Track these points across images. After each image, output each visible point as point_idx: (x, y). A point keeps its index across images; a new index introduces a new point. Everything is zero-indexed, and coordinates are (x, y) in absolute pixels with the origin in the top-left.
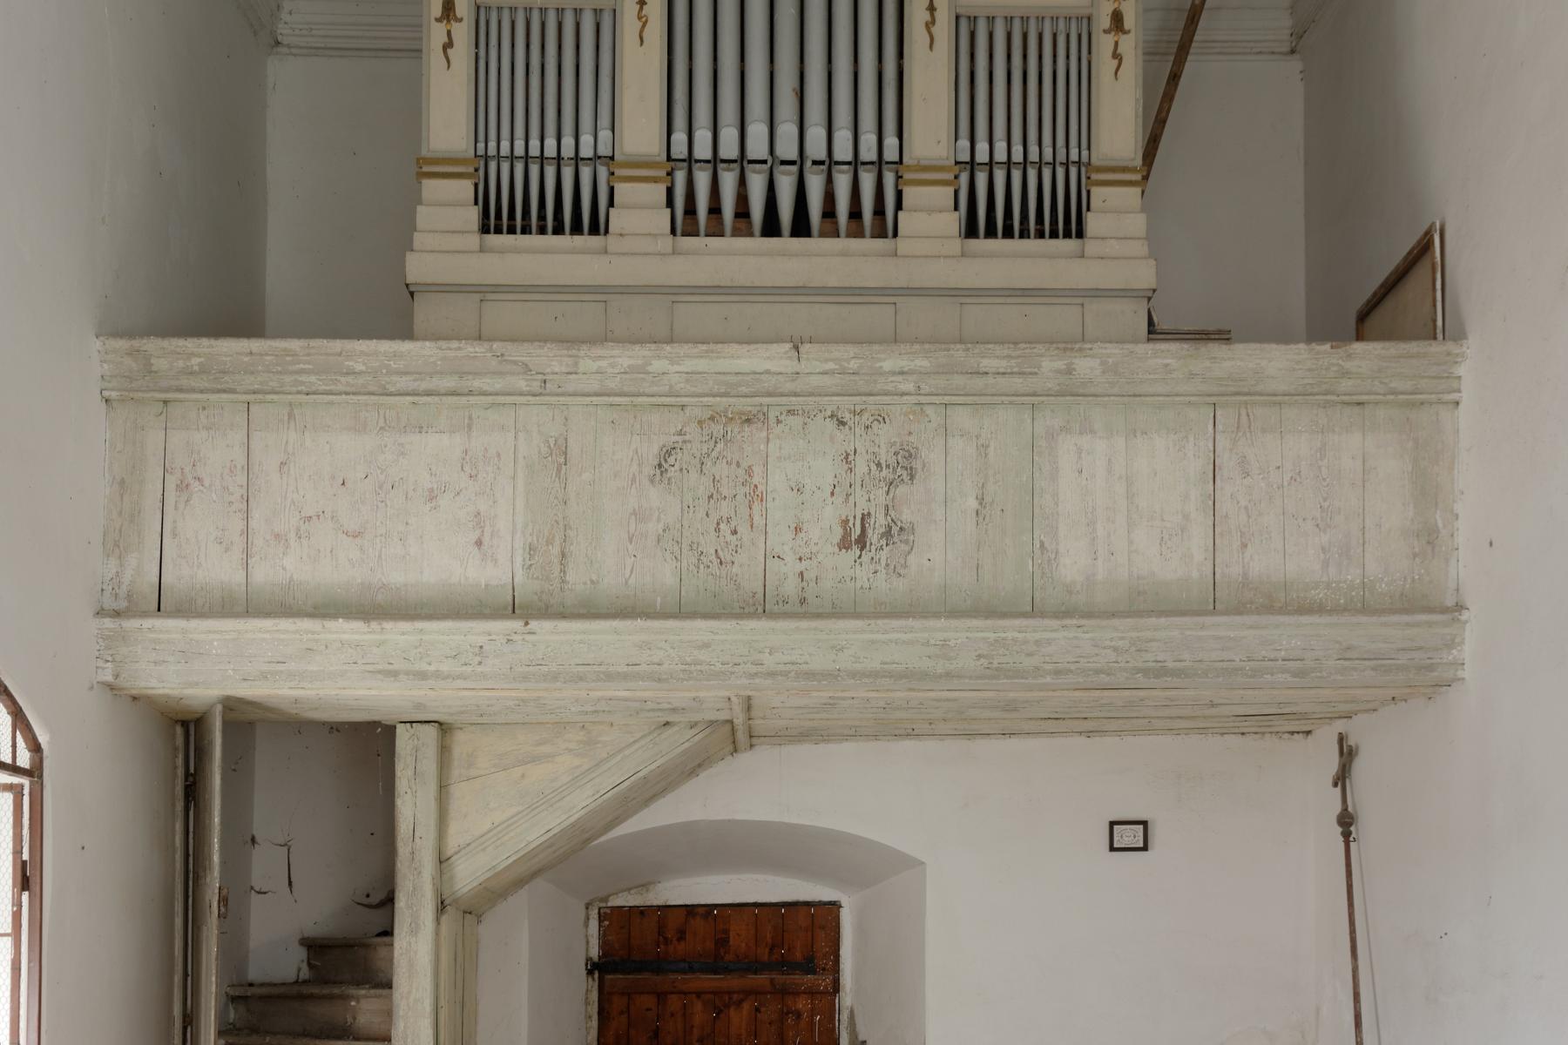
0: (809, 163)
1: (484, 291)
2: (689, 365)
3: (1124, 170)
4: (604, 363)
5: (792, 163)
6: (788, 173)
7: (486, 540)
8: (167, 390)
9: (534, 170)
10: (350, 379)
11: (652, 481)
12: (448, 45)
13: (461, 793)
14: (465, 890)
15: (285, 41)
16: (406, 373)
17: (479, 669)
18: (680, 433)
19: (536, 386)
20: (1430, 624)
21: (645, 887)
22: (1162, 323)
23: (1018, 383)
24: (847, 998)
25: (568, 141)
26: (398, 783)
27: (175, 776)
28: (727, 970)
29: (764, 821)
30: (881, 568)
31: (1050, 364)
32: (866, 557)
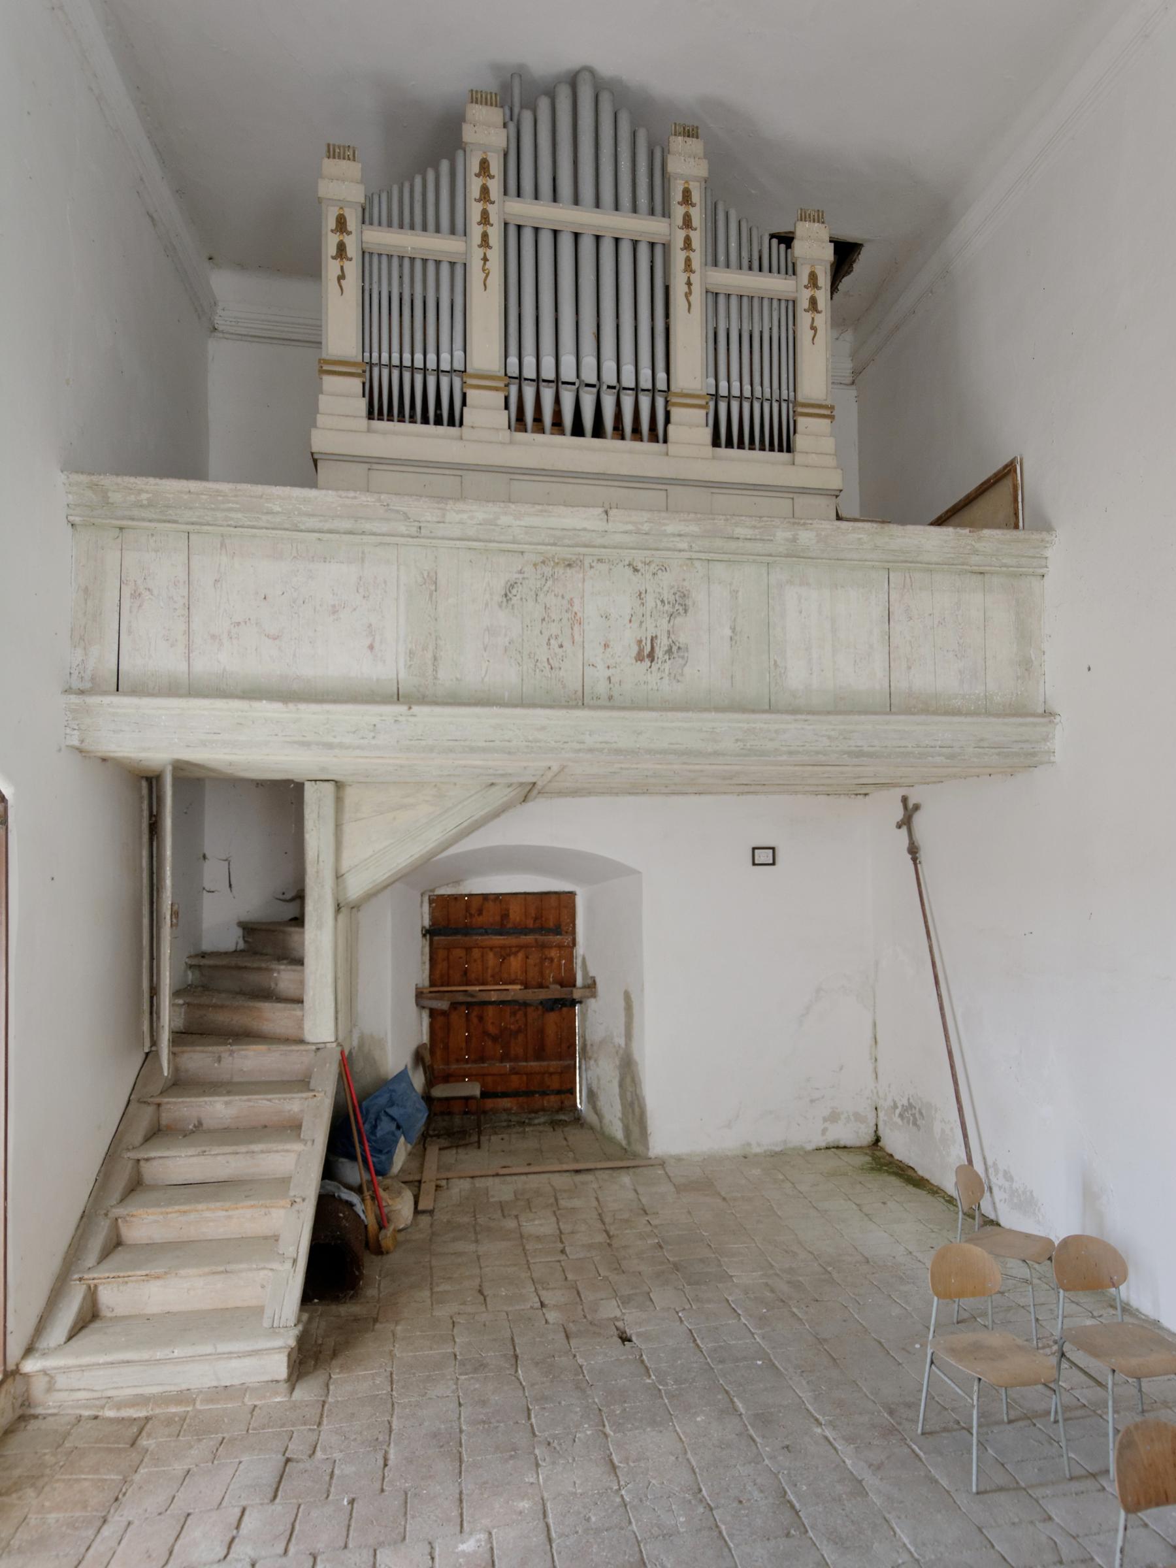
0: (605, 387)
1: (372, 462)
2: (528, 521)
3: (820, 406)
4: (465, 516)
5: (593, 386)
6: (590, 393)
7: (376, 645)
8: (123, 518)
10: (269, 517)
11: (500, 606)
12: (341, 277)
13: (348, 829)
14: (354, 897)
15: (220, 328)
16: (313, 515)
17: (373, 742)
18: (520, 572)
19: (413, 531)
21: (457, 882)
22: (842, 513)
24: (580, 950)
26: (306, 823)
27: (141, 816)
28: (508, 934)
30: (665, 675)
31: (782, 535)
32: (655, 666)
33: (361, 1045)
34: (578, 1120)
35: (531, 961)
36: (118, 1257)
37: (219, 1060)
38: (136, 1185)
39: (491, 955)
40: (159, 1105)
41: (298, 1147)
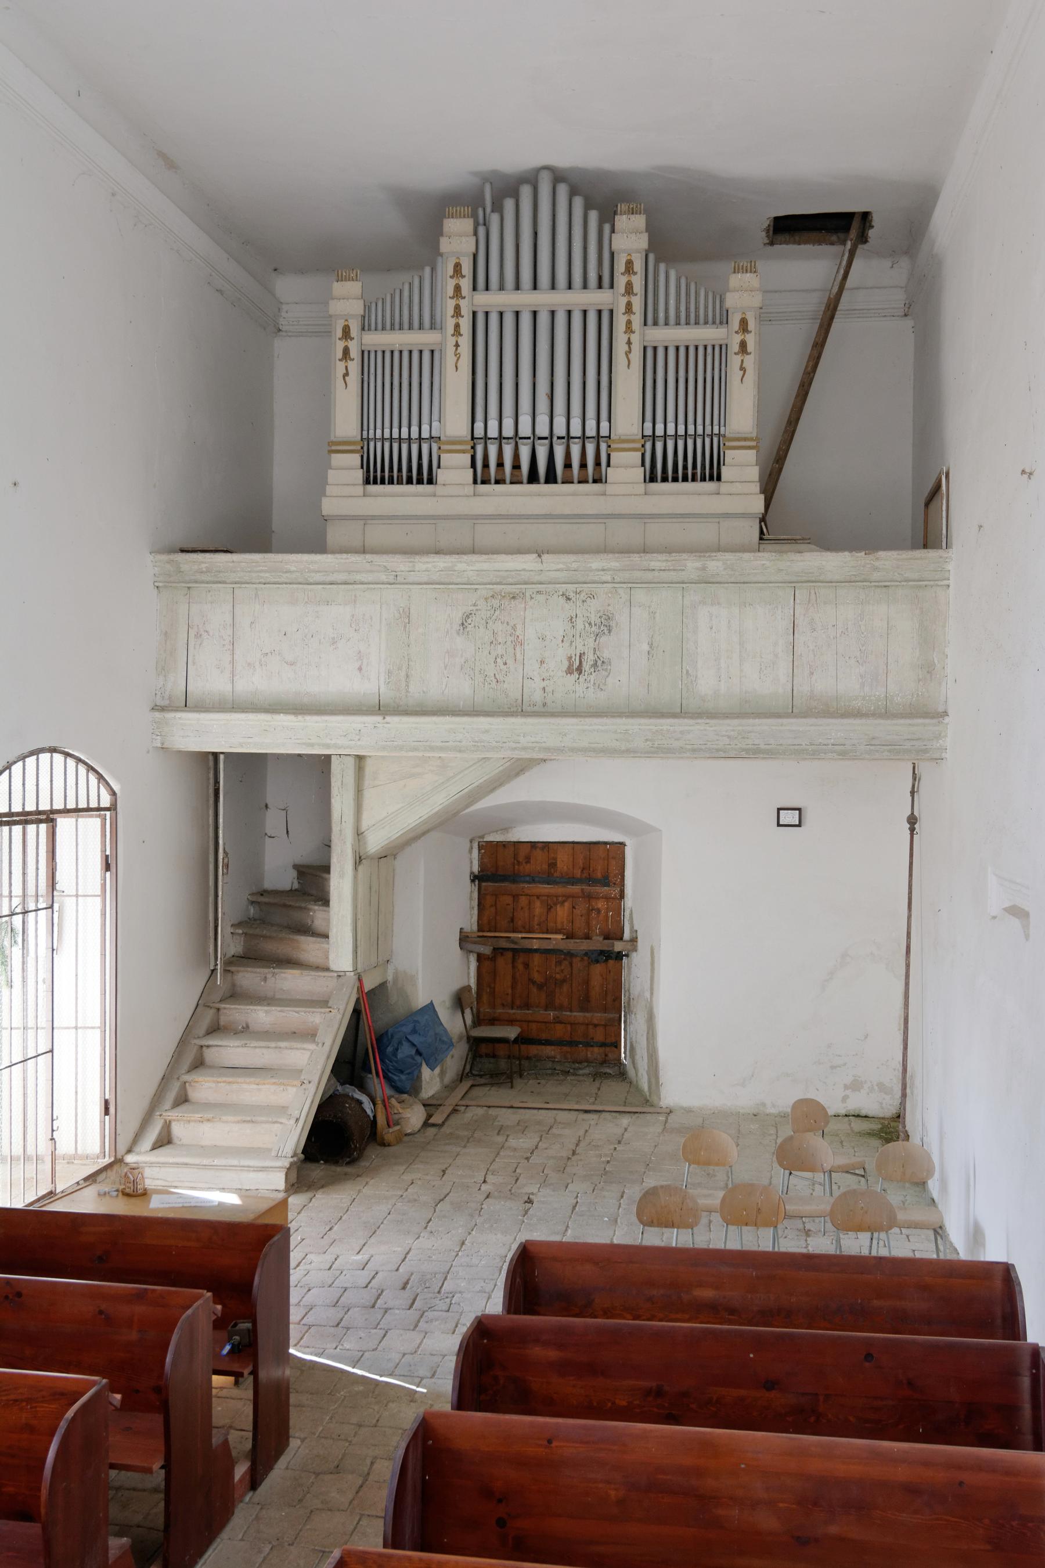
0: (555, 439)
2: (478, 566)
3: (745, 439)
4: (430, 566)
5: (546, 438)
7: (364, 667)
9: (395, 446)
10: (288, 575)
11: (458, 634)
12: (346, 374)
13: (368, 794)
15: (284, 328)
17: (359, 743)
18: (475, 605)
19: (391, 579)
20: (925, 725)
21: (506, 830)
23: (672, 576)
24: (629, 902)
25: (415, 429)
29: (564, 800)
30: (591, 685)
32: (582, 679)
33: (396, 980)
34: (622, 1074)
35: (577, 912)
36: (184, 1107)
37: (265, 979)
38: (199, 1064)
39: (538, 904)
40: (218, 1009)
41: (312, 1046)
